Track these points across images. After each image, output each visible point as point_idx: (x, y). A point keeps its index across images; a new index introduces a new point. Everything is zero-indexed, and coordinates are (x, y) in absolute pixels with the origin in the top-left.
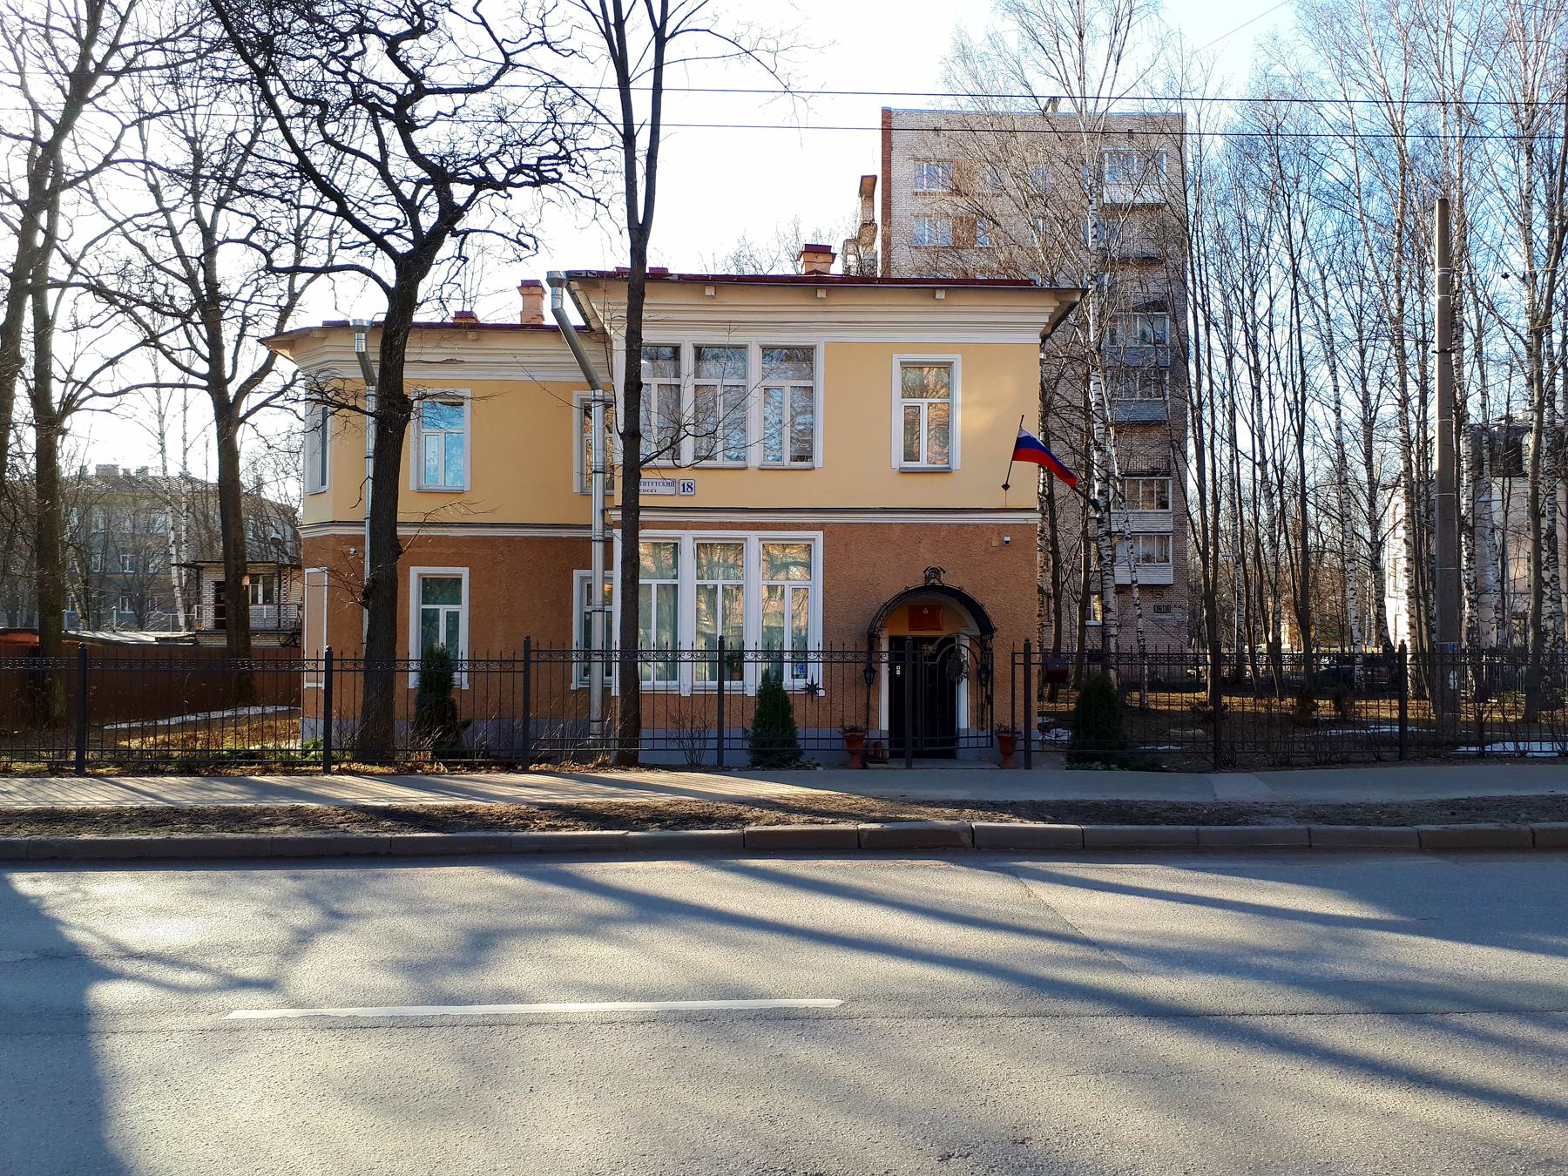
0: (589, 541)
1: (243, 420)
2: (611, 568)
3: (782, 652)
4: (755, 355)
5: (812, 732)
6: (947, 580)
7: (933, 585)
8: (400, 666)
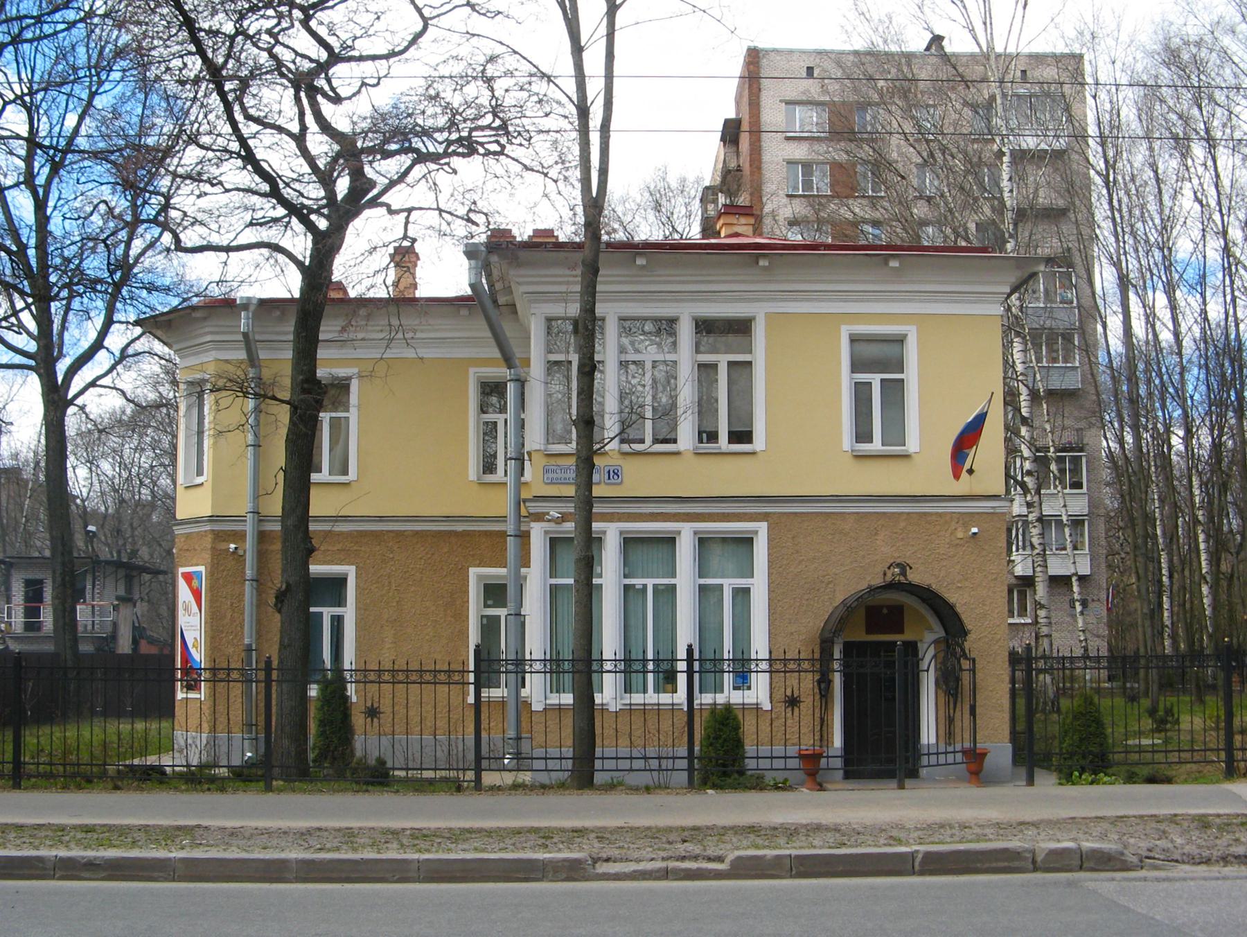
0: (503, 535)
1: (71, 402)
2: (527, 564)
3: (645, 660)
4: (686, 331)
5: (765, 750)
6: (914, 577)
7: (900, 583)
8: (595, 667)
